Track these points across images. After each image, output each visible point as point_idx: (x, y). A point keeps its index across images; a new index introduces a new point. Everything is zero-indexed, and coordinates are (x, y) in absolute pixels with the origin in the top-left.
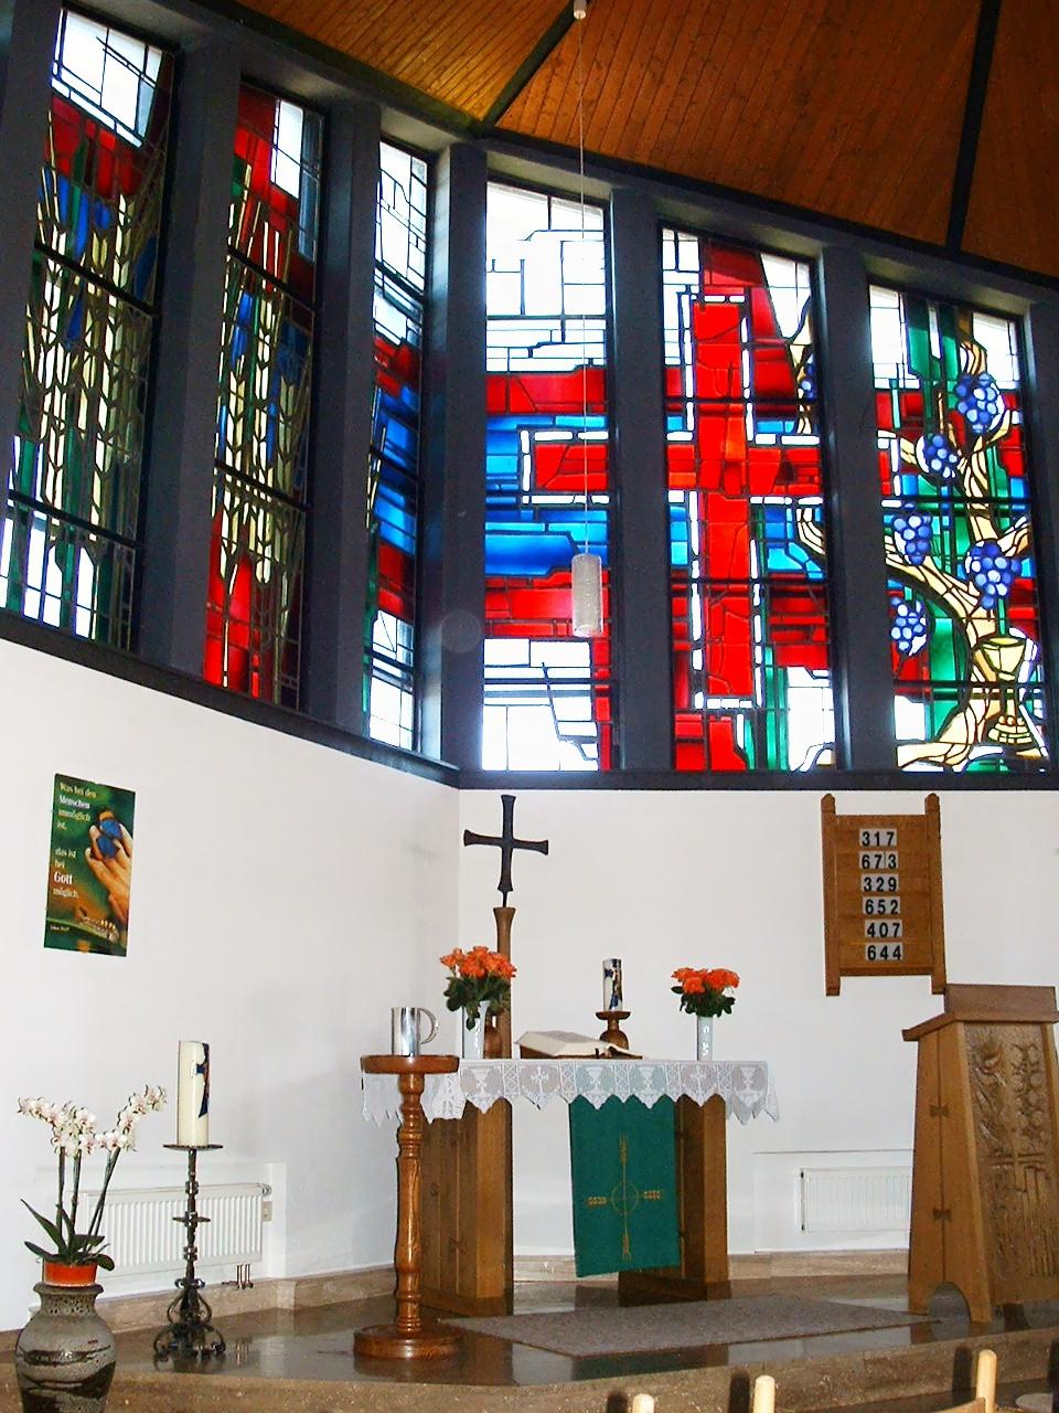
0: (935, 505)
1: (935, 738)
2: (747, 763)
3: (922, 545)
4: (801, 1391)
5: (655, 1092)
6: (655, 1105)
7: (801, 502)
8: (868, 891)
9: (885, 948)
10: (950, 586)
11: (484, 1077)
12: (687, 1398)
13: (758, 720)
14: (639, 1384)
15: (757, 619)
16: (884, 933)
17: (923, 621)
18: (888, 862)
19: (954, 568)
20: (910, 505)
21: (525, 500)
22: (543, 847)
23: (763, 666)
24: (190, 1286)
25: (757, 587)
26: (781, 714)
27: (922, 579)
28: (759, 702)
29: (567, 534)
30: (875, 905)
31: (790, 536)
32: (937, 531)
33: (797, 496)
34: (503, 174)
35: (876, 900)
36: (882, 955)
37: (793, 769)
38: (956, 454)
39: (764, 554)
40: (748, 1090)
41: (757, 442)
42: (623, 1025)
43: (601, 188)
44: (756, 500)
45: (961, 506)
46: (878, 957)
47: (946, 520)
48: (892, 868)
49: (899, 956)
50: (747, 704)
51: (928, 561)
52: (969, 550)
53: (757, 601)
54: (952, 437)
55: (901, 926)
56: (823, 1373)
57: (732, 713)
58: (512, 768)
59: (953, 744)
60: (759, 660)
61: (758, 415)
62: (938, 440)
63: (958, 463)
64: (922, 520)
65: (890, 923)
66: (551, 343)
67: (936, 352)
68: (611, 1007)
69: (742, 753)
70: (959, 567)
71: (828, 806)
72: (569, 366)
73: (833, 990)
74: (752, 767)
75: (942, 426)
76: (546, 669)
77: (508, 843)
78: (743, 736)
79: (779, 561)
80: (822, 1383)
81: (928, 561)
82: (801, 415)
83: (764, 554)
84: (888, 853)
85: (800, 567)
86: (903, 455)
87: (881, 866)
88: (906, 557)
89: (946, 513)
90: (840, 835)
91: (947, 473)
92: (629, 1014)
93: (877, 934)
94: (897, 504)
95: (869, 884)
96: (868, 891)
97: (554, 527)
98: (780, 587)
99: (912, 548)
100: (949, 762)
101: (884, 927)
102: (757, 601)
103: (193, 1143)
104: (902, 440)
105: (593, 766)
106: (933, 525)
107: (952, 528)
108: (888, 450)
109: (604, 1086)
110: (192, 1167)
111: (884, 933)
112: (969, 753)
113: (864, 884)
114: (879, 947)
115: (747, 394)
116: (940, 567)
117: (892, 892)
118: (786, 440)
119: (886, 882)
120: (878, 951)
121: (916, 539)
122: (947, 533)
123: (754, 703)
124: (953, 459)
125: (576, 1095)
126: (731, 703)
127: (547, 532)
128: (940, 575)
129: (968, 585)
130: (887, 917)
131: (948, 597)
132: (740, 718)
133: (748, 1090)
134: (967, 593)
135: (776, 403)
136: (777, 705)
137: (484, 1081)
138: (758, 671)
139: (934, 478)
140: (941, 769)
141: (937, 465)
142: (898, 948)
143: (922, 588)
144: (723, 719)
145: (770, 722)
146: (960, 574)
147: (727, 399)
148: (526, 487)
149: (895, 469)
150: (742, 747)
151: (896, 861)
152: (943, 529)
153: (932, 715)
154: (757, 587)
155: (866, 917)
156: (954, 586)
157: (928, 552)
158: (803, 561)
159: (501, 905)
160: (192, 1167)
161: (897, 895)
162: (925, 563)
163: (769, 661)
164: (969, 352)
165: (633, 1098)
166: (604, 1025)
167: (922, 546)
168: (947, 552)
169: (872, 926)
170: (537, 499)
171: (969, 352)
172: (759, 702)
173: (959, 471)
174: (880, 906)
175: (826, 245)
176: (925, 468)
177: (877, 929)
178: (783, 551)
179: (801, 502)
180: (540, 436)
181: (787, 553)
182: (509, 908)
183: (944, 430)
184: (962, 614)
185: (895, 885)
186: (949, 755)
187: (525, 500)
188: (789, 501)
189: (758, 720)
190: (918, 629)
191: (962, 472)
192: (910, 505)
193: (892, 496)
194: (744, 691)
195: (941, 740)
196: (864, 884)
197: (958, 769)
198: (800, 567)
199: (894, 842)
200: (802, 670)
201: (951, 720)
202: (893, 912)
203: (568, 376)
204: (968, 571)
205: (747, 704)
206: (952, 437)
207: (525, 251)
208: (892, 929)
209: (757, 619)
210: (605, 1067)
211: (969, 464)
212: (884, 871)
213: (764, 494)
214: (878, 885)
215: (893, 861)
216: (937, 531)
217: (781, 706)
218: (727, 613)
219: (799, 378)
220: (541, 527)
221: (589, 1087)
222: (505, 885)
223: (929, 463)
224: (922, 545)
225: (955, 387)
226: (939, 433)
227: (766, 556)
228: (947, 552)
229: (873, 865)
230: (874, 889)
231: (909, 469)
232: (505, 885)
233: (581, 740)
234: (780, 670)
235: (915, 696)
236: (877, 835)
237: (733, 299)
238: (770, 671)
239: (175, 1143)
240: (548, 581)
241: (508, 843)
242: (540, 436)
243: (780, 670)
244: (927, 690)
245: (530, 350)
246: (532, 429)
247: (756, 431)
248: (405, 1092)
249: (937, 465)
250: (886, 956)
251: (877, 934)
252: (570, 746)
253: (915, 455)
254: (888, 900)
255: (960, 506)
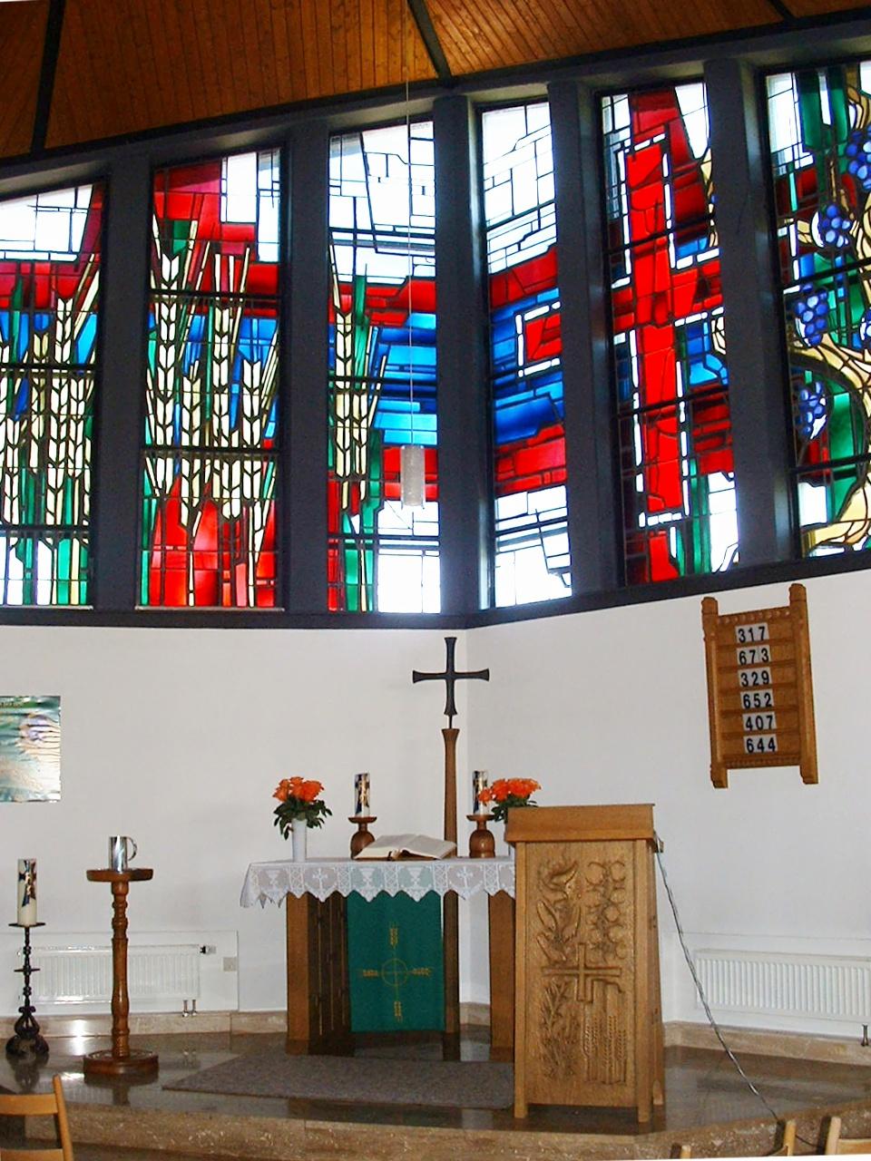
0: (831, 279)
1: (834, 519)
2: (678, 570)
3: (820, 323)
4: (244, 1142)
5: (280, 890)
6: (327, 899)
7: (714, 313)
8: (746, 686)
9: (761, 741)
10: (846, 358)
11: (276, 876)
12: (145, 1128)
13: (686, 528)
14: (110, 1111)
15: (684, 435)
16: (760, 726)
17: (823, 401)
18: (762, 655)
19: (850, 338)
20: (808, 287)
21: (521, 374)
22: (418, 677)
23: (689, 478)
24: (27, 1010)
25: (682, 405)
26: (704, 519)
27: (821, 358)
28: (687, 512)
29: (548, 395)
30: (752, 699)
31: (706, 349)
32: (833, 305)
33: (709, 309)
34: (490, 102)
35: (751, 694)
36: (759, 748)
37: (714, 570)
38: (849, 219)
39: (687, 373)
40: (275, 889)
41: (679, 267)
42: (371, 827)
43: (540, 89)
44: (679, 323)
45: (854, 272)
46: (756, 750)
47: (841, 292)
48: (765, 662)
49: (773, 747)
50: (678, 516)
51: (826, 339)
52: (863, 317)
53: (682, 418)
54: (844, 202)
55: (774, 717)
56: (265, 1131)
57: (665, 527)
58: (519, 603)
59: (853, 522)
60: (685, 473)
61: (678, 243)
62: (831, 210)
63: (850, 228)
64: (819, 298)
65: (763, 715)
66: (532, 233)
67: (827, 120)
68: (476, 808)
69: (673, 561)
70: (855, 335)
71: (709, 609)
72: (543, 249)
73: (719, 782)
74: (682, 573)
75: (835, 194)
76: (538, 514)
77: (451, 676)
78: (675, 547)
79: (701, 375)
80: (263, 1138)
81: (826, 339)
82: (712, 230)
83: (687, 373)
84: (761, 647)
85: (715, 376)
86: (800, 237)
87: (756, 660)
88: (806, 340)
89: (840, 284)
90: (719, 630)
91: (841, 242)
92: (375, 819)
93: (755, 728)
94: (796, 289)
95: (745, 679)
96: (746, 686)
97: (540, 391)
98: (702, 399)
99: (811, 330)
100: (850, 541)
101: (759, 721)
102: (682, 418)
103: (27, 923)
104: (799, 222)
105: (568, 593)
106: (829, 300)
107: (846, 299)
108: (788, 236)
109: (374, 883)
110: (27, 936)
111: (760, 726)
112: (868, 530)
113: (741, 680)
114: (756, 739)
115: (669, 225)
116: (837, 341)
117: (766, 685)
118: (701, 258)
119: (760, 676)
120: (755, 743)
121: (813, 321)
122: (842, 305)
123: (683, 514)
124: (846, 225)
125: (350, 891)
126: (666, 517)
127: (536, 397)
128: (837, 350)
129: (863, 354)
130: (763, 710)
131: (846, 371)
132: (673, 530)
133: (275, 889)
134: (863, 361)
135: (691, 227)
136: (700, 512)
137: (276, 879)
138: (685, 483)
139: (829, 251)
140: (842, 550)
141: (830, 237)
142: (772, 740)
143: (822, 368)
144: (660, 533)
145: (696, 530)
146: (856, 344)
147: (654, 236)
148: (521, 363)
149: (794, 254)
150: (675, 556)
151: (769, 654)
152: (838, 300)
153: (832, 497)
154: (682, 405)
155: (744, 712)
156: (851, 357)
157: (827, 329)
158: (717, 369)
159: (448, 727)
160: (27, 936)
161: (769, 688)
162: (824, 341)
163: (694, 472)
164: (858, 106)
165: (354, 893)
166: (355, 828)
167: (823, 321)
168: (843, 324)
169: (749, 719)
170: (529, 371)
171: (858, 106)
172: (687, 512)
173: (852, 235)
174: (755, 699)
175: (703, 61)
176: (820, 243)
177: (753, 723)
178: (701, 365)
179: (714, 313)
180: (529, 316)
181: (706, 367)
182: (455, 730)
183: (837, 198)
184: (859, 385)
185: (767, 678)
186: (850, 534)
187: (521, 374)
188: (705, 315)
189: (686, 528)
190: (819, 410)
191: (854, 235)
192: (808, 287)
193: (794, 284)
194: (676, 506)
195: (843, 519)
196: (741, 680)
197: (857, 547)
198: (715, 376)
199: (766, 636)
200: (720, 474)
201: (850, 499)
202: (768, 705)
203: (545, 256)
204: (863, 338)
205: (678, 516)
206: (844, 202)
207: (512, 160)
208: (766, 722)
209: (684, 435)
210: (376, 868)
211: (862, 226)
212: (758, 665)
213: (685, 317)
214: (753, 680)
215: (766, 655)
216: (833, 305)
217: (704, 513)
218: (661, 434)
219: (709, 193)
220: (530, 394)
221: (361, 883)
222: (451, 710)
223: (823, 238)
224: (820, 323)
225: (846, 150)
226: (831, 203)
227: (689, 374)
228: (843, 324)
229: (749, 661)
230: (751, 684)
231: (806, 249)
232: (451, 710)
233: (561, 571)
234: (702, 479)
235: (816, 481)
236: (751, 631)
237: (656, 139)
238: (694, 481)
239: (16, 922)
240: (538, 439)
241: (451, 676)
242: (529, 316)
243: (702, 479)
244: (828, 470)
245: (519, 243)
246: (522, 312)
247: (678, 258)
248: (114, 892)
249: (830, 237)
250: (762, 748)
251: (755, 728)
252: (555, 578)
253: (810, 234)
254: (762, 693)
255: (852, 273)
